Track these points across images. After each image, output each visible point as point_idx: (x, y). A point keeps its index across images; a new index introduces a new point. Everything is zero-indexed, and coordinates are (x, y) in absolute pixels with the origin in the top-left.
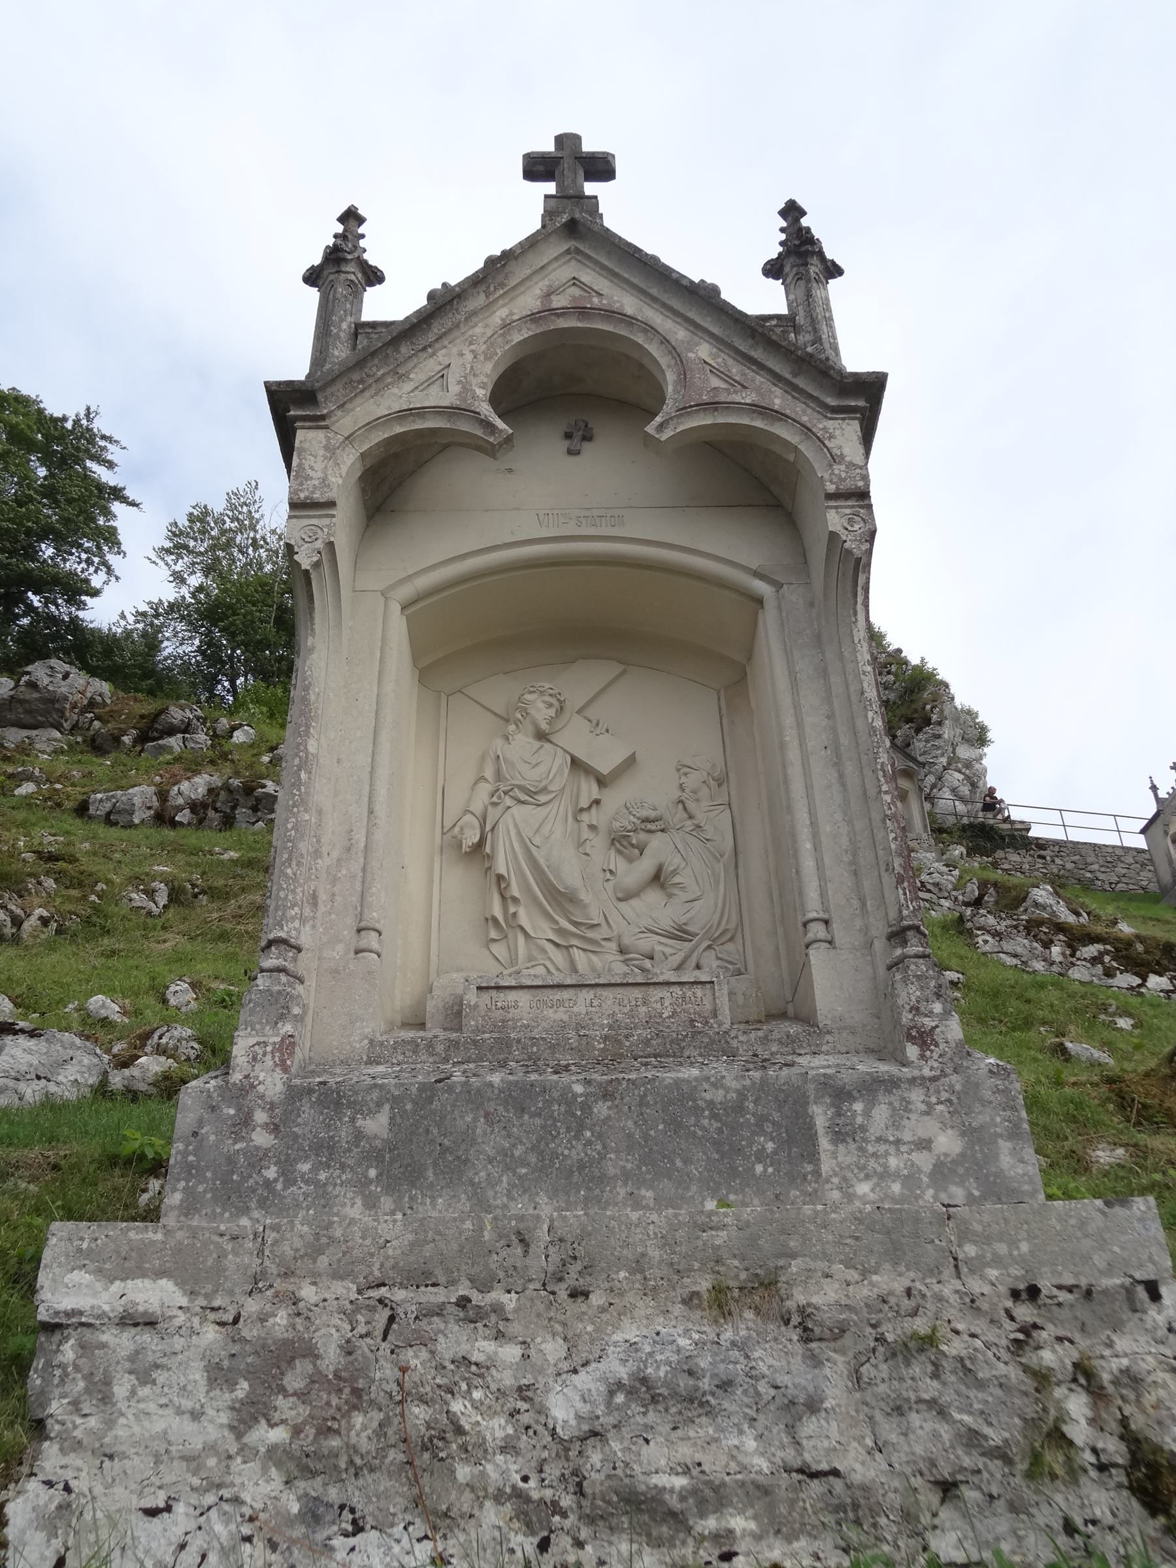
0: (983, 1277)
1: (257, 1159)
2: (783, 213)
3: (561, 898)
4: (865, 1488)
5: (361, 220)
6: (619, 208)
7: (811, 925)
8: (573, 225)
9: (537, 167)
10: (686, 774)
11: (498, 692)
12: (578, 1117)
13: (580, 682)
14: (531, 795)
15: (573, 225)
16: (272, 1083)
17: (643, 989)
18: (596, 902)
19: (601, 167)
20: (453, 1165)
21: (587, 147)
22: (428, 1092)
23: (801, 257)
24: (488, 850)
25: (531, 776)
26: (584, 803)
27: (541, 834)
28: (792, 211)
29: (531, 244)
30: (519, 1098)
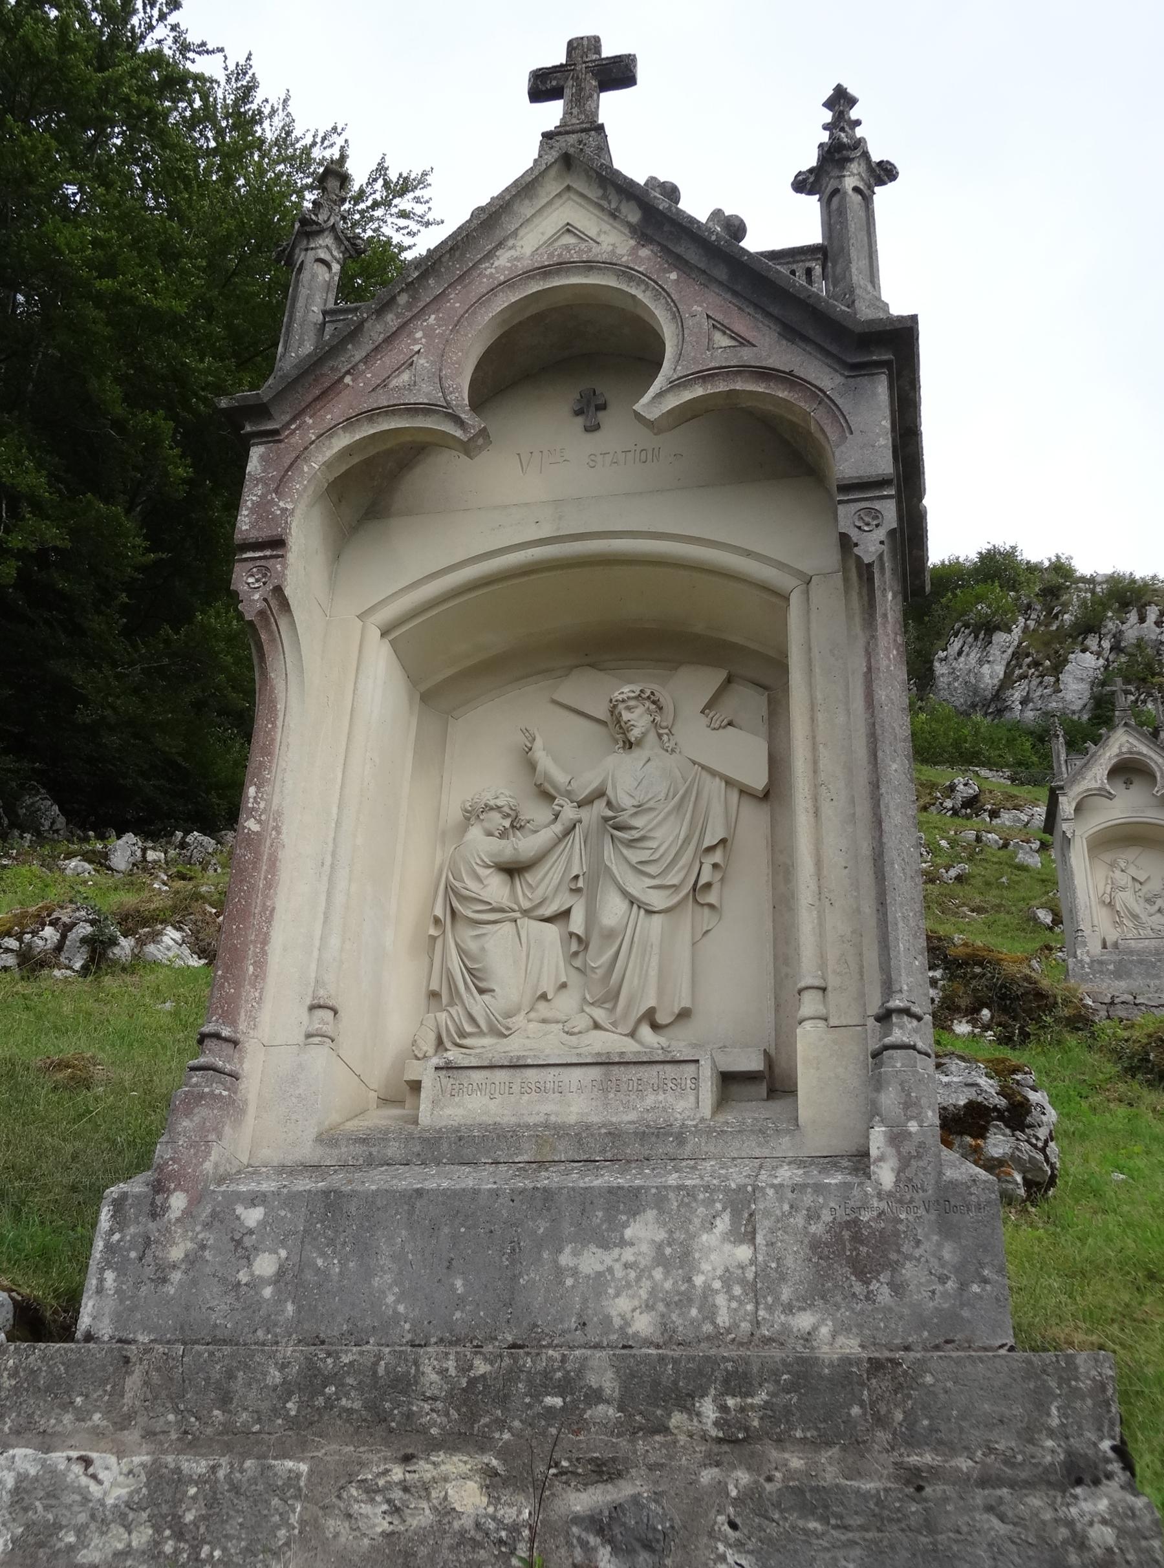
1: (1088, 974)
2: (829, 104)
3: (1135, 917)
4: (187, 1256)
5: (852, 102)
6: (638, 136)
8: (576, 156)
9: (543, 86)
11: (1108, 857)
12: (1153, 965)
13: (1131, 854)
14: (1123, 889)
15: (576, 156)
16: (1087, 959)
18: (1144, 917)
19: (619, 73)
20: (1129, 975)
21: (609, 50)
22: (1121, 961)
23: (842, 169)
25: (1123, 883)
27: (1127, 899)
28: (840, 100)
29: (524, 188)
30: (1141, 962)
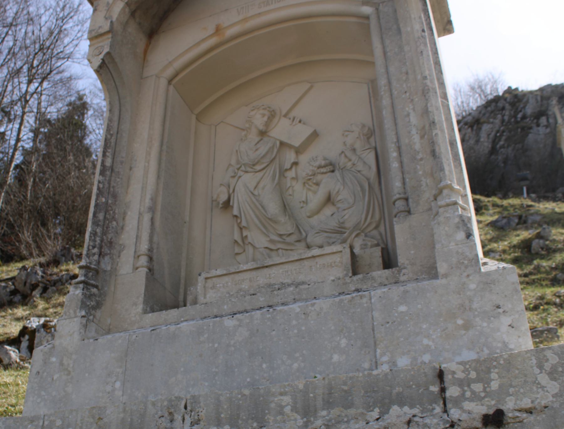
0: (461, 408)
7: (397, 203)
10: (347, 136)
17: (297, 263)
24: (231, 204)
26: (287, 166)
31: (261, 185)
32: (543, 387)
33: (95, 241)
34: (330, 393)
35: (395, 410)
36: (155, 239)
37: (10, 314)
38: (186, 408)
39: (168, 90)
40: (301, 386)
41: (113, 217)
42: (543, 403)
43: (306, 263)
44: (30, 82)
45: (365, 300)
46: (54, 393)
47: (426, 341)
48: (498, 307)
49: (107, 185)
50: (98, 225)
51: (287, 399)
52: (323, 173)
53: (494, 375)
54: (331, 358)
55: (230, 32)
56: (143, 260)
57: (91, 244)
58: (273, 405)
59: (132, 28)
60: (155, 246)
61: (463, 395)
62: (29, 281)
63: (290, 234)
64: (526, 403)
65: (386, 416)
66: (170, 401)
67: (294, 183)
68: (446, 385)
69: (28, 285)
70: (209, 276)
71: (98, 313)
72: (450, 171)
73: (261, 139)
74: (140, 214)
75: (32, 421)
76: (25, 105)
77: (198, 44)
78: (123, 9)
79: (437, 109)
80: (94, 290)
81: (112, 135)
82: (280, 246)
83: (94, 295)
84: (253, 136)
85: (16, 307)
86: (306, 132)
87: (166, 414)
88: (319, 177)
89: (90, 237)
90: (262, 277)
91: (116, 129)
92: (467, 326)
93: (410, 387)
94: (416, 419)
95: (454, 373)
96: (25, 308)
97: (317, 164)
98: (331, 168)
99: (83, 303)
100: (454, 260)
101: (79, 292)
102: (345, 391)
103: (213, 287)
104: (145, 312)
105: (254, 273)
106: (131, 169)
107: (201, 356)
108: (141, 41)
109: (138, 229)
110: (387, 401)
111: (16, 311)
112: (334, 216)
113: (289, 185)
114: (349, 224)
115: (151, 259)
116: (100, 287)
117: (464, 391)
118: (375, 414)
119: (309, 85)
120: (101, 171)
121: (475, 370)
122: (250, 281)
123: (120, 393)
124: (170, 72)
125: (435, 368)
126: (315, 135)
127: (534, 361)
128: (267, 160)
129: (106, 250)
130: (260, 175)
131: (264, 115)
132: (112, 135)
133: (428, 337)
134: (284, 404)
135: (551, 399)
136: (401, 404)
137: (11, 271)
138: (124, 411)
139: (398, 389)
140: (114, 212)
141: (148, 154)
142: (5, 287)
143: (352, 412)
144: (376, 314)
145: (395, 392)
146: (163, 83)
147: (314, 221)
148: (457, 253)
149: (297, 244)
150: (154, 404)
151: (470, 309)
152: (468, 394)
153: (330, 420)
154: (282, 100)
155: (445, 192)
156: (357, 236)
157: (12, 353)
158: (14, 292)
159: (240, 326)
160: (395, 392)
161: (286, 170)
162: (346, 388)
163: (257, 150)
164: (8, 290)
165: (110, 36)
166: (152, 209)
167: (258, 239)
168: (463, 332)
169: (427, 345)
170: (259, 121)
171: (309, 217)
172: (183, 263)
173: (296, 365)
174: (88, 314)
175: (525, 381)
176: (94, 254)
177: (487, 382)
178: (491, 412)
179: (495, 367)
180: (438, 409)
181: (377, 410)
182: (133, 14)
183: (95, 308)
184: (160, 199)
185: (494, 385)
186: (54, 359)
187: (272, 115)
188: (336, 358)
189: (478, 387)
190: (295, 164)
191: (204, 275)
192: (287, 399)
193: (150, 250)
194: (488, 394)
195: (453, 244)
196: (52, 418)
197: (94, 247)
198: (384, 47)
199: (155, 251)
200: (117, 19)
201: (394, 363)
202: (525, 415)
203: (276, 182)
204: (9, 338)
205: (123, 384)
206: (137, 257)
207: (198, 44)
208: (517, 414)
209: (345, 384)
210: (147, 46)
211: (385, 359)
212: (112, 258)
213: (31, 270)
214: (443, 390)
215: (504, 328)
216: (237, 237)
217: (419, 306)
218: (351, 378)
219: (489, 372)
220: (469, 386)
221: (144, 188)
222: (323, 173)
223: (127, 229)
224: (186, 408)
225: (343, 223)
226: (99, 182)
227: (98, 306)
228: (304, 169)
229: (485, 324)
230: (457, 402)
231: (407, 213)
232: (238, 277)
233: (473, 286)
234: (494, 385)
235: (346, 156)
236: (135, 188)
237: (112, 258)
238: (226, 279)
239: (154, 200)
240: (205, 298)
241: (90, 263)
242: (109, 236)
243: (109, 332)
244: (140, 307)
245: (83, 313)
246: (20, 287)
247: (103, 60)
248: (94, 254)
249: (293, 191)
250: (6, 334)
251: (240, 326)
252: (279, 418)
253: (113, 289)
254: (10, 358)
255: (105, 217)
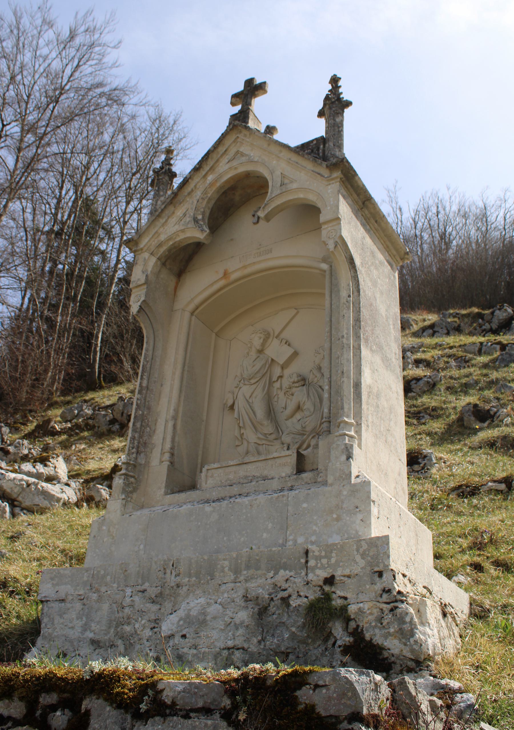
0: (314, 573)
17: (264, 462)
26: (275, 378)
31: (254, 395)
32: (357, 563)
33: (134, 443)
34: (249, 561)
35: (282, 572)
36: (177, 439)
37: (108, 446)
38: (173, 566)
39: (190, 320)
40: (235, 556)
41: (148, 425)
42: (356, 572)
43: (270, 462)
44: (128, 203)
45: (285, 498)
46: (104, 551)
47: (314, 528)
48: (357, 507)
49: (143, 401)
50: (136, 432)
51: (226, 563)
52: (296, 387)
53: (334, 555)
54: (262, 536)
55: (234, 277)
56: (167, 456)
57: (131, 446)
58: (219, 566)
59: (165, 275)
60: (176, 445)
61: (317, 565)
62: (126, 412)
63: (271, 434)
64: (347, 572)
65: (277, 576)
66: (165, 561)
67: (279, 392)
68: (309, 559)
69: (124, 415)
70: (209, 468)
71: (135, 495)
72: (349, 409)
73: (258, 357)
74: (166, 421)
75: (87, 571)
76: (124, 226)
77: (212, 285)
78: (156, 262)
79: (348, 360)
80: (132, 480)
81: (147, 362)
82: (264, 442)
83: (132, 483)
84: (253, 354)
85: (113, 439)
86: (289, 351)
87: (162, 569)
88: (294, 390)
89: (131, 441)
90: (242, 471)
91: (151, 357)
92: (338, 519)
93: (291, 559)
94: (292, 578)
95: (314, 552)
96: (121, 439)
97: (292, 380)
98: (302, 383)
99: (124, 489)
100: (338, 474)
101: (121, 481)
102: (257, 560)
103: (212, 476)
104: (166, 494)
105: (237, 467)
106: (162, 385)
107: (190, 530)
108: (172, 281)
109: (165, 432)
110: (278, 567)
111: (113, 442)
112: (300, 421)
113: (275, 394)
114: (309, 429)
115: (172, 454)
116: (136, 477)
117: (318, 563)
118: (271, 574)
119: (296, 311)
120: (139, 391)
121: (325, 551)
122: (235, 473)
123: (143, 552)
124: (191, 307)
125: (304, 548)
126: (296, 354)
127: (355, 547)
128: (259, 375)
129: (142, 449)
130: (254, 386)
131: (260, 338)
132: (147, 362)
133: (316, 525)
134: (225, 566)
135: (360, 570)
136: (285, 569)
137: (112, 396)
138: (139, 566)
139: (284, 560)
140: (148, 421)
141: (174, 374)
142: (105, 416)
143: (259, 572)
144: (290, 508)
145: (282, 561)
146: (187, 315)
147: (289, 423)
148: (340, 469)
149: (275, 441)
150: (156, 563)
151: (342, 508)
152: (319, 565)
153: (248, 577)
154: (275, 324)
155: (342, 425)
156: (313, 437)
157: (102, 491)
158: (113, 421)
159: (214, 511)
160: (282, 561)
161: (274, 382)
162: (257, 558)
163: (254, 366)
164: (108, 419)
165: (145, 287)
166: (175, 418)
167: (251, 436)
168: (336, 523)
169: (315, 530)
170: (257, 342)
171: (286, 420)
172: (200, 453)
173: (242, 539)
174: (127, 496)
175: (349, 559)
176: (133, 453)
177: (329, 558)
178: (329, 576)
179: (335, 550)
180: (303, 573)
181: (272, 572)
182: (164, 264)
183: (131, 492)
184: (181, 409)
185: (333, 560)
186: (104, 528)
187: (267, 336)
188: (265, 535)
189: (324, 561)
190: (281, 377)
191: (206, 467)
192: (226, 563)
193: (172, 448)
194: (329, 566)
195: (338, 463)
196: (99, 569)
197: (133, 448)
198: (331, 300)
199: (176, 448)
200: (151, 272)
201: (295, 541)
202: (346, 579)
203: (265, 392)
204: (103, 474)
205: (145, 547)
206: (162, 453)
207: (212, 285)
208: (342, 578)
209: (257, 555)
210: (177, 283)
211: (291, 538)
212: (146, 455)
213: (128, 401)
214: (307, 562)
215: (358, 522)
216: (237, 433)
217: (314, 504)
218: (261, 552)
219: (331, 552)
220: (320, 560)
221: (169, 402)
222: (296, 387)
223: (157, 432)
224: (173, 566)
225: (304, 428)
226: (138, 399)
227: (135, 490)
228: (286, 382)
229: (348, 518)
230: (313, 569)
231: (328, 433)
232: (228, 470)
233: (345, 493)
234: (333, 560)
235: (313, 374)
236: (164, 400)
237: (146, 455)
238: (220, 470)
239: (176, 411)
240: (206, 484)
241: (130, 460)
242: (145, 438)
243: (142, 507)
244: (163, 490)
245: (123, 497)
246: (118, 417)
247: (140, 306)
248: (133, 453)
249: (278, 398)
250: (101, 469)
251: (214, 511)
252: (222, 574)
253: (146, 476)
254: (101, 496)
255: (141, 425)
